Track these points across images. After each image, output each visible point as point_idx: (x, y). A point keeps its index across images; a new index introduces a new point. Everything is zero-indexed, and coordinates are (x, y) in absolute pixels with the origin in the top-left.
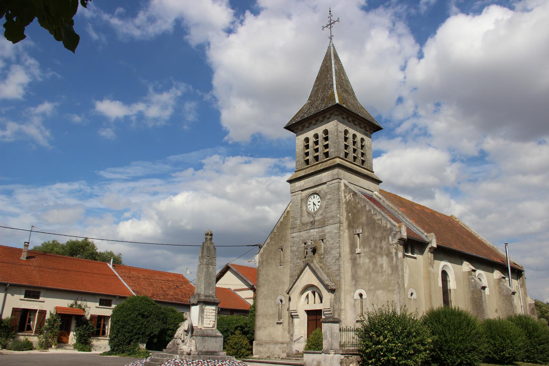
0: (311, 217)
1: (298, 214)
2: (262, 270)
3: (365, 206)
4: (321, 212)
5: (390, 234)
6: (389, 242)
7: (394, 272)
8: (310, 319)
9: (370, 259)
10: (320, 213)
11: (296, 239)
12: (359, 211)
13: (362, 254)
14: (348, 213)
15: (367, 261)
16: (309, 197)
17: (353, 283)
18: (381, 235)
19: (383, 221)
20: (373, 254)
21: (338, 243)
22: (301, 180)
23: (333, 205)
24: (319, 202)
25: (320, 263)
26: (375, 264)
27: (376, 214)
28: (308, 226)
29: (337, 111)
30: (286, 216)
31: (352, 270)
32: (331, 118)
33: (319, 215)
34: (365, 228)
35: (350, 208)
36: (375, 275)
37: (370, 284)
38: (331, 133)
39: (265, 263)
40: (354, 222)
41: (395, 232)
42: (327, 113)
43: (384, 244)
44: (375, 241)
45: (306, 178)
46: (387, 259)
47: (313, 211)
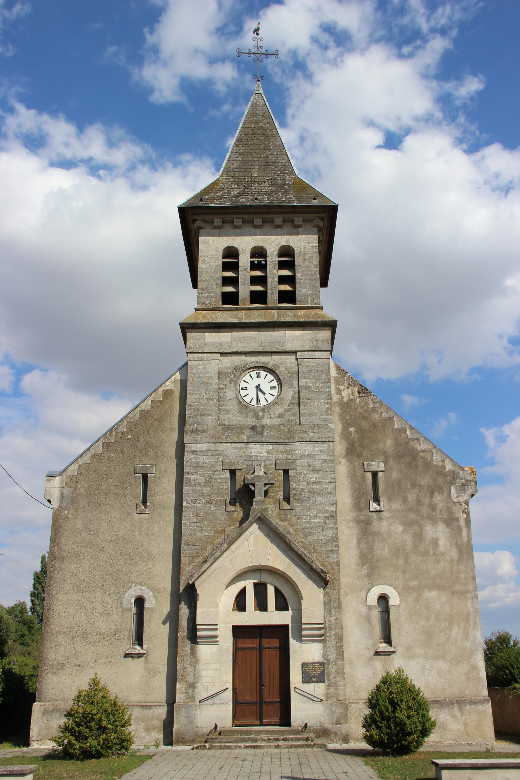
0: (249, 417)
1: (211, 402)
2: (70, 516)
3: (391, 419)
4: (279, 410)
5: (452, 483)
6: (450, 497)
7: (465, 556)
8: (240, 645)
9: (407, 525)
10: (277, 412)
11: (201, 458)
12: (375, 426)
13: (385, 514)
14: (346, 425)
15: (399, 528)
16: (244, 371)
17: (365, 570)
18: (431, 483)
19: (434, 455)
20: (412, 516)
21: (330, 482)
22: (223, 330)
23: (316, 403)
24: (272, 388)
25: (281, 521)
26: (419, 537)
27: (418, 439)
28: (242, 433)
29: (322, 219)
30: (161, 402)
31: (359, 543)
32: (303, 228)
33: (273, 416)
34: (391, 462)
35: (351, 416)
36: (420, 558)
37: (407, 575)
38: (302, 258)
39: (82, 503)
40: (363, 447)
41: (463, 480)
42: (298, 215)
43: (438, 499)
44: (416, 490)
45: (239, 330)
46: (447, 530)
47: (254, 403)
